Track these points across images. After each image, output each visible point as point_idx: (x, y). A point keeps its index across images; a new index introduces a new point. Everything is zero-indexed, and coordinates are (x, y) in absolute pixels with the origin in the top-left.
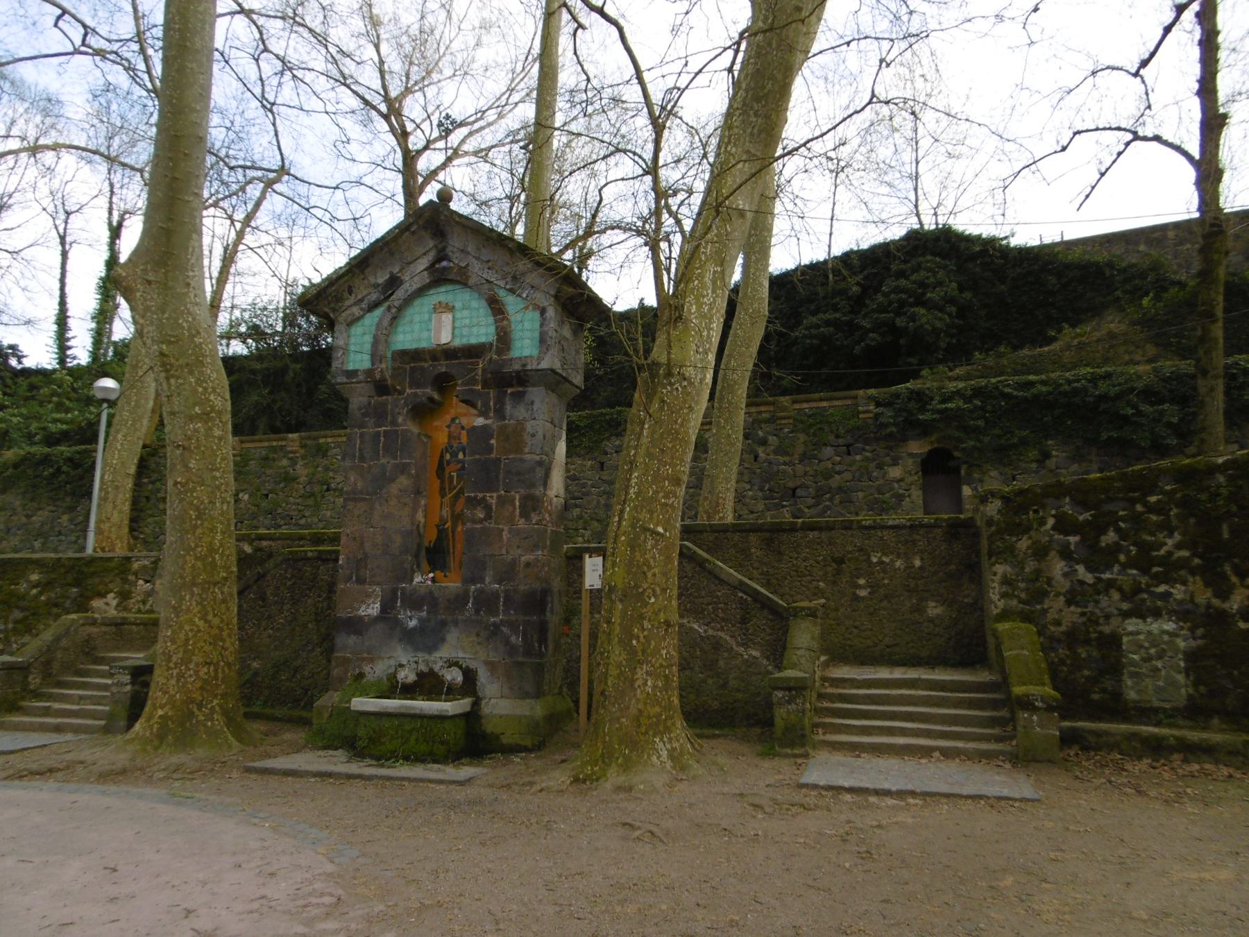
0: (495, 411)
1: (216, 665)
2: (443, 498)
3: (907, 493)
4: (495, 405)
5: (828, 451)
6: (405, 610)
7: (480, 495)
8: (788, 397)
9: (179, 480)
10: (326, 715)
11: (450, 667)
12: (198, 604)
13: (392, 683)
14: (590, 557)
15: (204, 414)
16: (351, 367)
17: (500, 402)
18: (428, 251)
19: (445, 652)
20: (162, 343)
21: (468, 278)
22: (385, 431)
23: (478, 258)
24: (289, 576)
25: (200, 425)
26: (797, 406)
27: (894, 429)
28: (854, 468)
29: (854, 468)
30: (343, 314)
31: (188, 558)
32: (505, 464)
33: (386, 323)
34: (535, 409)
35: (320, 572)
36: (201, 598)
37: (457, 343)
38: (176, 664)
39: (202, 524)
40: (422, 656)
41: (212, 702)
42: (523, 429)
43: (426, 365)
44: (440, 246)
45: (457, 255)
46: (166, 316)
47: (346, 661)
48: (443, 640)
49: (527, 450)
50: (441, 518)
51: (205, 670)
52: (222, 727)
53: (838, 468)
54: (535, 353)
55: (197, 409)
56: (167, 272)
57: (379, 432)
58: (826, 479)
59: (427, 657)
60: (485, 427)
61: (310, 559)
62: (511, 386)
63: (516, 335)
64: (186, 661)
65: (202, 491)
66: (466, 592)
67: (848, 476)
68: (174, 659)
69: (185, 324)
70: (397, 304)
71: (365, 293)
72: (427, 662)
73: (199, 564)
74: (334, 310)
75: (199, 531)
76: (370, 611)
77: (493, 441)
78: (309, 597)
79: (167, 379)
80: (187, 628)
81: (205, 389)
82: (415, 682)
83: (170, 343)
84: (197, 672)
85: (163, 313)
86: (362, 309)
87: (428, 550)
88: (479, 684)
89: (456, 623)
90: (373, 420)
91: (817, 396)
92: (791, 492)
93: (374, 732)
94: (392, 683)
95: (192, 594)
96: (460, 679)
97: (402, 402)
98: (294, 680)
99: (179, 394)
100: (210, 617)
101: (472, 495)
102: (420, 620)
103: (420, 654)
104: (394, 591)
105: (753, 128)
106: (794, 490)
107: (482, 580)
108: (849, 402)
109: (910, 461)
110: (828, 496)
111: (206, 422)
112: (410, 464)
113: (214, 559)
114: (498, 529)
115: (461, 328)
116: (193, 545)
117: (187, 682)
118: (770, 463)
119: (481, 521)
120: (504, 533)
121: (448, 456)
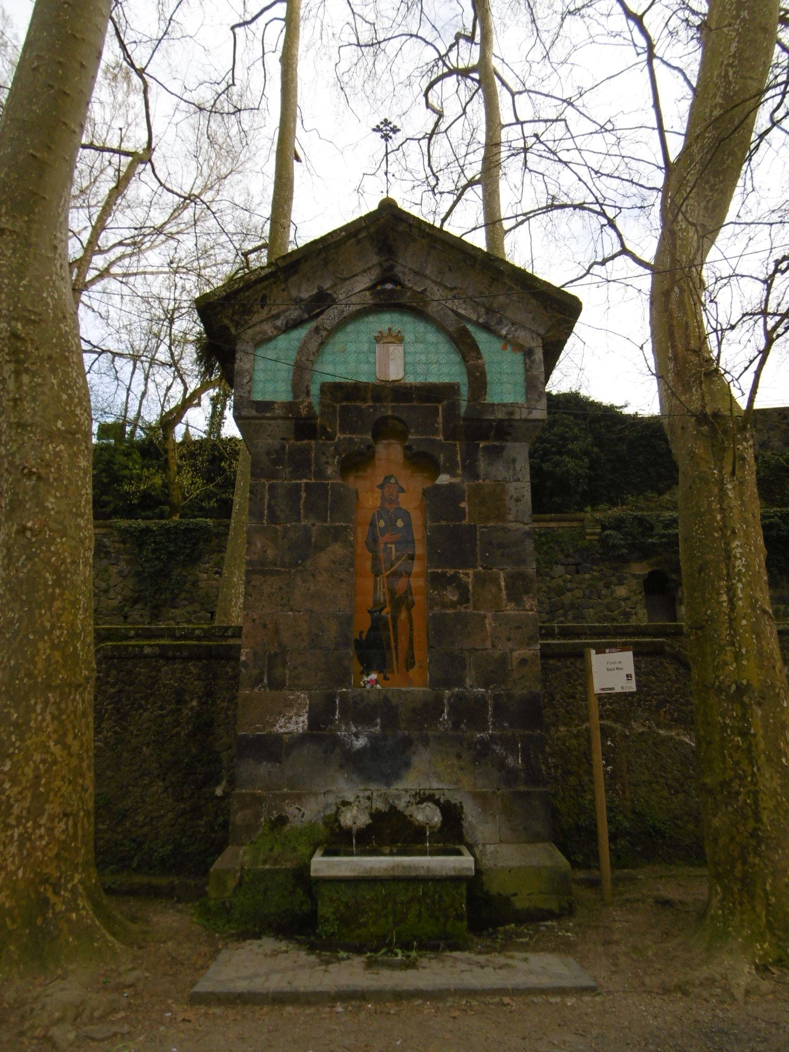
0: (464, 467)
1: (75, 815)
2: (377, 576)
3: (633, 611)
4: (463, 460)
5: (559, 570)
6: (347, 725)
7: (450, 572)
9: (29, 524)
10: (232, 883)
11: (421, 802)
12: (54, 718)
13: (332, 830)
14: (597, 653)
15: (70, 433)
16: (258, 397)
17: (470, 455)
18: (369, 269)
19: (410, 782)
20: (17, 320)
22: (307, 485)
23: (440, 284)
24: (111, 680)
25: (62, 447)
27: (625, 551)
28: (584, 586)
29: (584, 586)
30: (250, 332)
31: (41, 645)
32: (482, 533)
33: (313, 346)
34: (518, 469)
36: (59, 709)
37: (410, 380)
38: (19, 818)
39: (62, 594)
40: (376, 789)
41: (72, 878)
43: (364, 406)
44: (386, 265)
45: (411, 277)
46: (24, 282)
47: (257, 800)
48: (407, 765)
49: (511, 517)
50: (376, 603)
51: (62, 825)
52: (93, 921)
53: (569, 585)
54: (521, 400)
55: (59, 423)
56: (30, 221)
57: (299, 485)
58: (559, 596)
59: (384, 789)
60: (451, 486)
61: (146, 656)
62: (486, 438)
63: (491, 376)
64: (34, 813)
65: (63, 544)
66: (438, 700)
67: (579, 593)
68: (16, 810)
69: (49, 300)
70: (328, 324)
71: (282, 308)
72: (385, 798)
73: (57, 655)
74: (237, 325)
75: (57, 604)
76: (292, 727)
77: (463, 505)
78: (145, 710)
79: (17, 374)
80: (37, 757)
81: (71, 397)
82: (368, 826)
83: (28, 322)
84: (50, 830)
85: (21, 279)
86: (276, 328)
87: (358, 644)
88: (465, 824)
89: (426, 742)
90: (288, 470)
91: (548, 516)
93: (347, 906)
94: (332, 830)
95: (46, 703)
96: (437, 819)
97: (332, 449)
98: (119, 829)
99: (34, 399)
100: (69, 739)
101: (440, 571)
102: (371, 737)
103: (373, 786)
104: (330, 698)
105: (708, 201)
107: (460, 682)
108: (575, 524)
109: (634, 581)
110: (561, 611)
111: (70, 445)
113: (75, 648)
114: (479, 615)
115: (414, 364)
116: (48, 625)
117: (34, 848)
119: (453, 605)
120: (487, 621)
121: (382, 524)
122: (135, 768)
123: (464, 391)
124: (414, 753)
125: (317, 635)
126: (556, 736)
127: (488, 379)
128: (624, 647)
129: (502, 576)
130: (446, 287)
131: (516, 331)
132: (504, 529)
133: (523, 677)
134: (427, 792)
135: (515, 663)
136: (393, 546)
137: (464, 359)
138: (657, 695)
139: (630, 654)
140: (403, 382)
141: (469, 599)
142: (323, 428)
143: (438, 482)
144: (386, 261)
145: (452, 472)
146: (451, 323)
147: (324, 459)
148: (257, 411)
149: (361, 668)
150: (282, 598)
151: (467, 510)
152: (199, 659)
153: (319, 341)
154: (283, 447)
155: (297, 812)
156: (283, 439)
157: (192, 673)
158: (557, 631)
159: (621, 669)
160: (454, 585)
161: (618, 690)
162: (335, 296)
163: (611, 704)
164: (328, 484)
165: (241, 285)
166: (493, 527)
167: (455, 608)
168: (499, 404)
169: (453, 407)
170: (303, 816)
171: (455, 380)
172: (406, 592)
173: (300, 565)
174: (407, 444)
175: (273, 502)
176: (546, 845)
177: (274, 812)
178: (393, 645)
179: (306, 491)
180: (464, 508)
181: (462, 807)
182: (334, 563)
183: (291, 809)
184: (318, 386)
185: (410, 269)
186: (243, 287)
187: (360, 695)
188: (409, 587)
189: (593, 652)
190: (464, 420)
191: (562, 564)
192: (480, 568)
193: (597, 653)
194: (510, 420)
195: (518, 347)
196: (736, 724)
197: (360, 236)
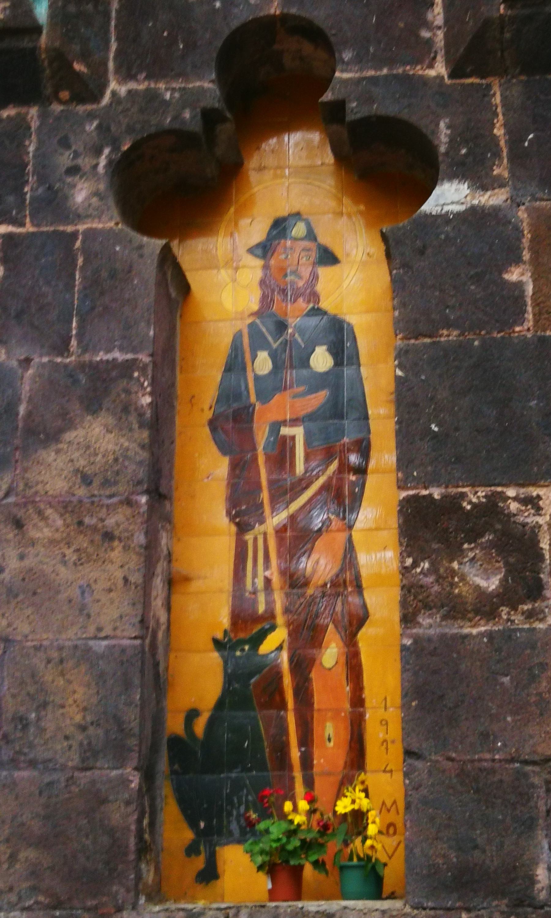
97: (92, 127)
101: (437, 493)
151: (529, 289)
160: (488, 537)
164: (74, 235)
178: (295, 754)
180: (519, 285)
182: (87, 480)
196: (531, 742)
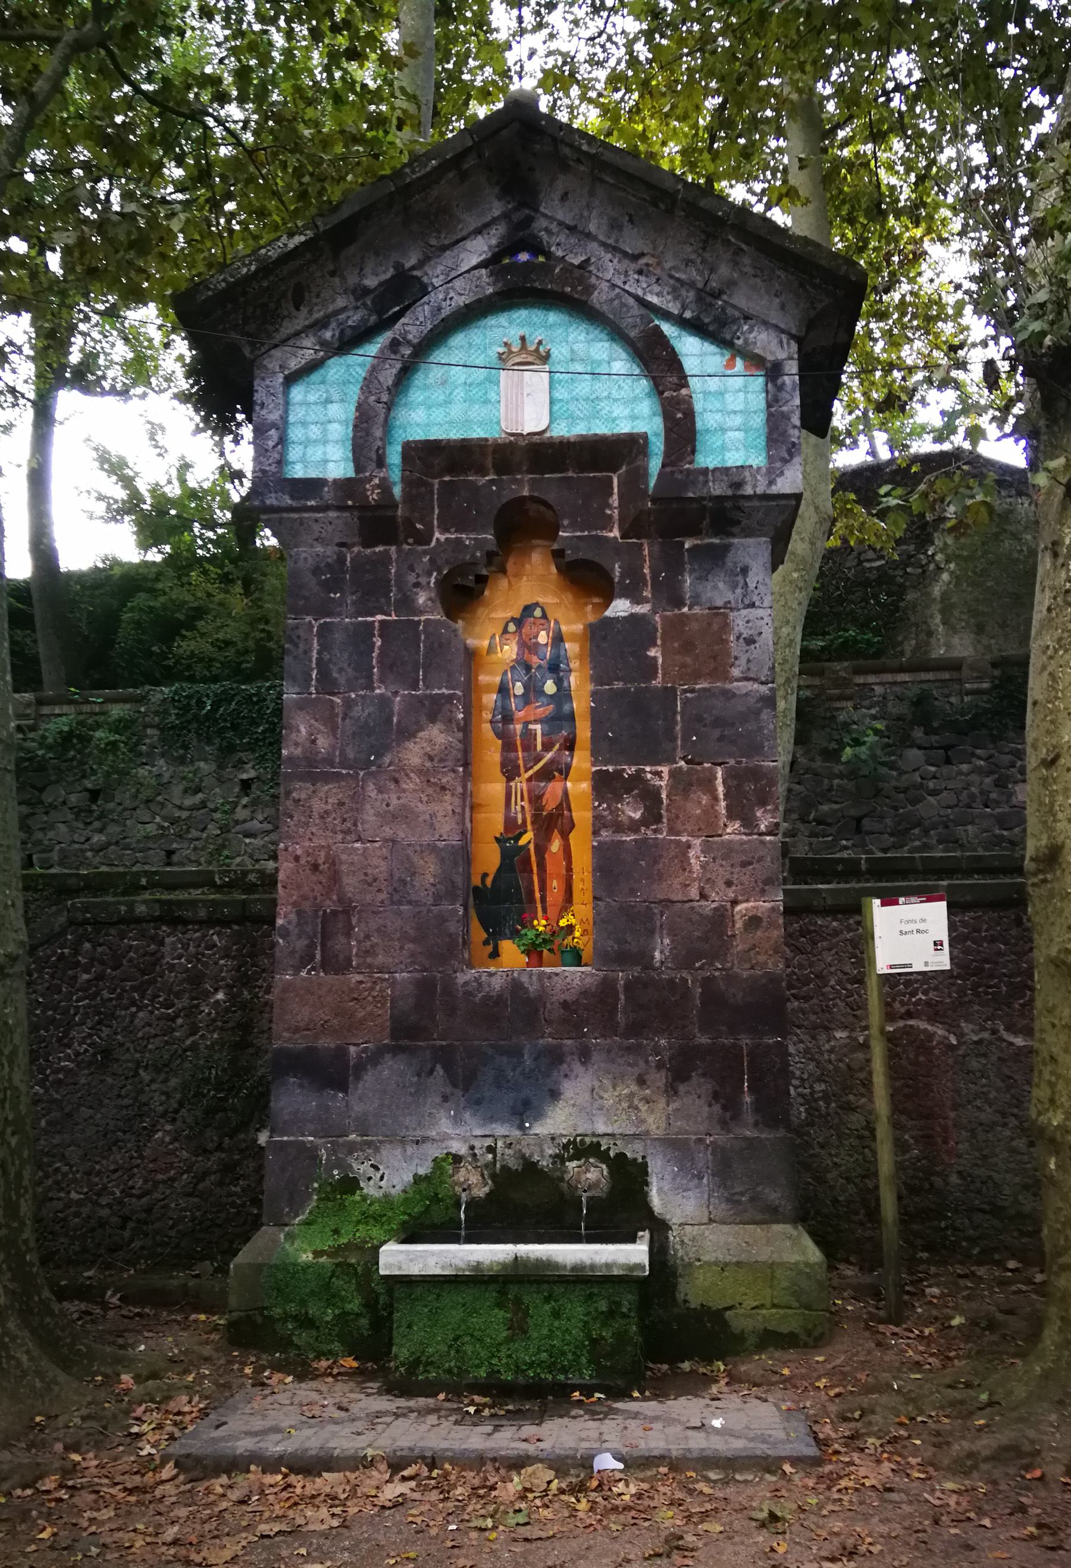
2: (510, 779)
5: (914, 755)
7: (630, 770)
8: (846, 664)
14: (883, 904)
16: (298, 472)
18: (487, 226)
21: (589, 289)
22: (381, 622)
23: (615, 249)
26: (860, 680)
32: (686, 702)
33: (388, 376)
34: (752, 586)
35: (166, 950)
37: (562, 431)
42: (726, 626)
44: (516, 217)
45: (562, 238)
48: (555, 1095)
49: (736, 672)
50: (510, 823)
54: (757, 459)
60: (633, 619)
61: (139, 920)
62: (693, 531)
70: (414, 334)
77: (652, 653)
78: (140, 1009)
92: (854, 824)
97: (426, 559)
101: (611, 769)
106: (859, 820)
112: (451, 697)
118: (816, 774)
119: (634, 826)
120: (692, 853)
122: (126, 1101)
123: (657, 446)
124: (566, 1076)
125: (403, 882)
126: (827, 1047)
127: (699, 425)
128: (929, 895)
129: (719, 775)
130: (625, 254)
131: (751, 331)
132: (729, 695)
133: (754, 947)
134: (588, 1140)
135: (739, 925)
136: (538, 728)
137: (658, 388)
138: (1010, 977)
139: (942, 905)
140: (548, 435)
141: (660, 816)
142: (409, 523)
143: (609, 613)
144: (516, 209)
145: (634, 596)
146: (632, 319)
147: (412, 578)
148: (292, 498)
149: (485, 936)
150: (344, 820)
151: (660, 661)
152: (224, 923)
153: (399, 365)
154: (341, 560)
155: (371, 1172)
156: (342, 545)
157: (215, 945)
158: (864, 866)
159: (926, 932)
161: (918, 967)
162: (425, 279)
163: (925, 993)
164: (419, 622)
165: (253, 268)
166: (704, 690)
167: (636, 831)
168: (716, 469)
169: (639, 475)
170: (382, 1178)
171: (640, 427)
172: (559, 807)
173: (373, 763)
174: (555, 547)
175: (326, 656)
176: (788, 1228)
177: (336, 1172)
178: (537, 895)
179: (380, 636)
180: (655, 658)
181: (645, 1165)
182: (431, 758)
183: (362, 1167)
184: (399, 448)
185: (561, 223)
186: (257, 271)
187: (476, 980)
188: (566, 793)
189: (877, 902)
190: (654, 501)
191: (920, 748)
192: (682, 763)
193: (883, 904)
194: (736, 498)
195: (755, 361)
197: (466, 166)
